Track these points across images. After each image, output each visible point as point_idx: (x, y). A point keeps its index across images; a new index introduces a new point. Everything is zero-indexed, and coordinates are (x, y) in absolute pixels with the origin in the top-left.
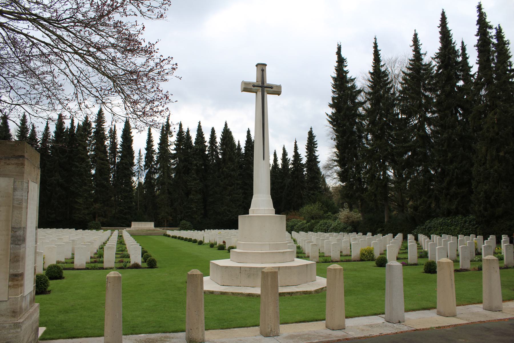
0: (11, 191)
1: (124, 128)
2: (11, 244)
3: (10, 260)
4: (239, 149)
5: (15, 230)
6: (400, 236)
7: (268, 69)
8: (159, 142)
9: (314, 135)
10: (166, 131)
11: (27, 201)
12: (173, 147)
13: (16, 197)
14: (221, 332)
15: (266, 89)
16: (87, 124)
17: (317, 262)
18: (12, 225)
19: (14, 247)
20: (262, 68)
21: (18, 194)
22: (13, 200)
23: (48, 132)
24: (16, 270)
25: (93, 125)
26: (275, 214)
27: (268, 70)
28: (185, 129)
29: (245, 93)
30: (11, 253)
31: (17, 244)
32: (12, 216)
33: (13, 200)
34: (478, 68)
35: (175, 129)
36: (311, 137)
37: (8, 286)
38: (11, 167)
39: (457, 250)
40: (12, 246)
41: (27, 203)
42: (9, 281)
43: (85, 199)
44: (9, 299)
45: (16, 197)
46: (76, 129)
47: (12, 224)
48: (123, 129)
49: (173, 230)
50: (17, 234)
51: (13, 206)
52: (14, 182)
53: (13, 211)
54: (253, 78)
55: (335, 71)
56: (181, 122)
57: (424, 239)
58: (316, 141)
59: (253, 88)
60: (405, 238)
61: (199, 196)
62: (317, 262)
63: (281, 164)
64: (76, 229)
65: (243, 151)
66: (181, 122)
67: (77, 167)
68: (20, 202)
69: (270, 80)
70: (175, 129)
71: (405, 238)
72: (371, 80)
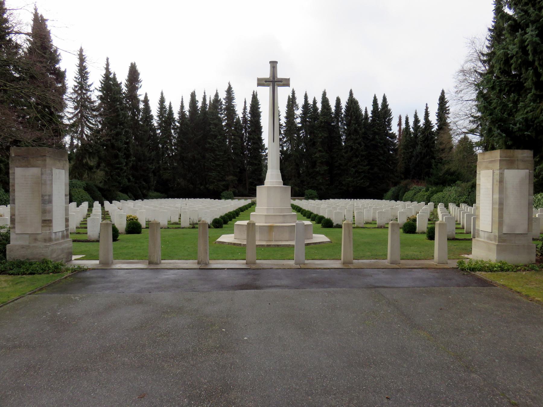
1: (251, 103)
2: (42, 204)
7: (278, 65)
8: (285, 115)
9: (446, 100)
10: (292, 102)
12: (298, 120)
15: (276, 83)
16: (217, 100)
20: (274, 64)
21: (44, 177)
23: (184, 111)
25: (224, 102)
26: (283, 185)
27: (279, 67)
28: (311, 102)
29: (259, 87)
35: (300, 102)
36: (442, 101)
38: (39, 162)
39: (353, 213)
40: (42, 205)
43: (367, 165)
44: (42, 233)
46: (208, 107)
48: (251, 105)
49: (301, 200)
51: (42, 183)
52: (42, 170)
54: (267, 75)
57: (465, 207)
58: (449, 107)
59: (265, 83)
61: (326, 168)
64: (215, 199)
67: (210, 143)
69: (280, 75)
70: (300, 102)
72: (489, 38)
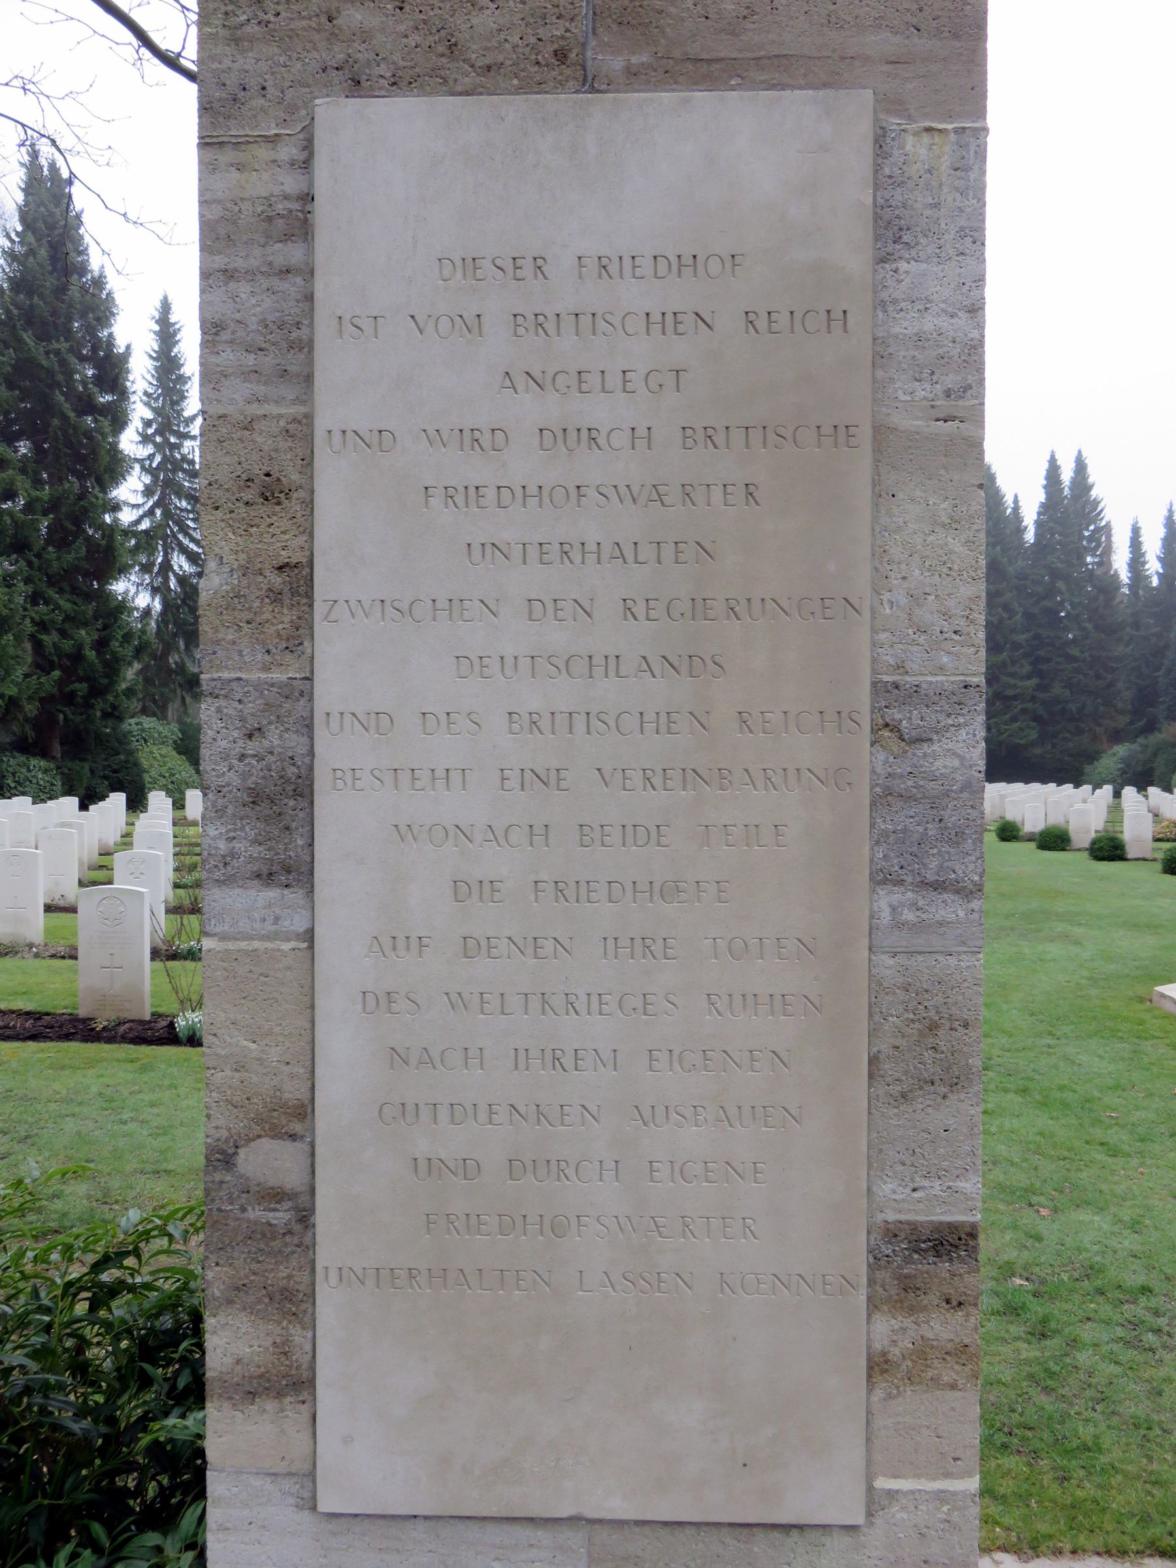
2: (882, 878)
3: (873, 1061)
4: (1020, 530)
5: (909, 719)
6: (1108, 789)
13: (905, 325)
14: (160, 1006)
18: (874, 671)
19: (909, 916)
22: (880, 355)
30: (877, 988)
31: (938, 886)
32: (880, 553)
37: (863, 1363)
40: (885, 900)
42: (873, 1305)
44: (874, 1502)
45: (905, 325)
51: (881, 432)
52: (881, 141)
53: (881, 494)
60: (1117, 794)
63: (1157, 573)
65: (1030, 536)
71: (1117, 794)
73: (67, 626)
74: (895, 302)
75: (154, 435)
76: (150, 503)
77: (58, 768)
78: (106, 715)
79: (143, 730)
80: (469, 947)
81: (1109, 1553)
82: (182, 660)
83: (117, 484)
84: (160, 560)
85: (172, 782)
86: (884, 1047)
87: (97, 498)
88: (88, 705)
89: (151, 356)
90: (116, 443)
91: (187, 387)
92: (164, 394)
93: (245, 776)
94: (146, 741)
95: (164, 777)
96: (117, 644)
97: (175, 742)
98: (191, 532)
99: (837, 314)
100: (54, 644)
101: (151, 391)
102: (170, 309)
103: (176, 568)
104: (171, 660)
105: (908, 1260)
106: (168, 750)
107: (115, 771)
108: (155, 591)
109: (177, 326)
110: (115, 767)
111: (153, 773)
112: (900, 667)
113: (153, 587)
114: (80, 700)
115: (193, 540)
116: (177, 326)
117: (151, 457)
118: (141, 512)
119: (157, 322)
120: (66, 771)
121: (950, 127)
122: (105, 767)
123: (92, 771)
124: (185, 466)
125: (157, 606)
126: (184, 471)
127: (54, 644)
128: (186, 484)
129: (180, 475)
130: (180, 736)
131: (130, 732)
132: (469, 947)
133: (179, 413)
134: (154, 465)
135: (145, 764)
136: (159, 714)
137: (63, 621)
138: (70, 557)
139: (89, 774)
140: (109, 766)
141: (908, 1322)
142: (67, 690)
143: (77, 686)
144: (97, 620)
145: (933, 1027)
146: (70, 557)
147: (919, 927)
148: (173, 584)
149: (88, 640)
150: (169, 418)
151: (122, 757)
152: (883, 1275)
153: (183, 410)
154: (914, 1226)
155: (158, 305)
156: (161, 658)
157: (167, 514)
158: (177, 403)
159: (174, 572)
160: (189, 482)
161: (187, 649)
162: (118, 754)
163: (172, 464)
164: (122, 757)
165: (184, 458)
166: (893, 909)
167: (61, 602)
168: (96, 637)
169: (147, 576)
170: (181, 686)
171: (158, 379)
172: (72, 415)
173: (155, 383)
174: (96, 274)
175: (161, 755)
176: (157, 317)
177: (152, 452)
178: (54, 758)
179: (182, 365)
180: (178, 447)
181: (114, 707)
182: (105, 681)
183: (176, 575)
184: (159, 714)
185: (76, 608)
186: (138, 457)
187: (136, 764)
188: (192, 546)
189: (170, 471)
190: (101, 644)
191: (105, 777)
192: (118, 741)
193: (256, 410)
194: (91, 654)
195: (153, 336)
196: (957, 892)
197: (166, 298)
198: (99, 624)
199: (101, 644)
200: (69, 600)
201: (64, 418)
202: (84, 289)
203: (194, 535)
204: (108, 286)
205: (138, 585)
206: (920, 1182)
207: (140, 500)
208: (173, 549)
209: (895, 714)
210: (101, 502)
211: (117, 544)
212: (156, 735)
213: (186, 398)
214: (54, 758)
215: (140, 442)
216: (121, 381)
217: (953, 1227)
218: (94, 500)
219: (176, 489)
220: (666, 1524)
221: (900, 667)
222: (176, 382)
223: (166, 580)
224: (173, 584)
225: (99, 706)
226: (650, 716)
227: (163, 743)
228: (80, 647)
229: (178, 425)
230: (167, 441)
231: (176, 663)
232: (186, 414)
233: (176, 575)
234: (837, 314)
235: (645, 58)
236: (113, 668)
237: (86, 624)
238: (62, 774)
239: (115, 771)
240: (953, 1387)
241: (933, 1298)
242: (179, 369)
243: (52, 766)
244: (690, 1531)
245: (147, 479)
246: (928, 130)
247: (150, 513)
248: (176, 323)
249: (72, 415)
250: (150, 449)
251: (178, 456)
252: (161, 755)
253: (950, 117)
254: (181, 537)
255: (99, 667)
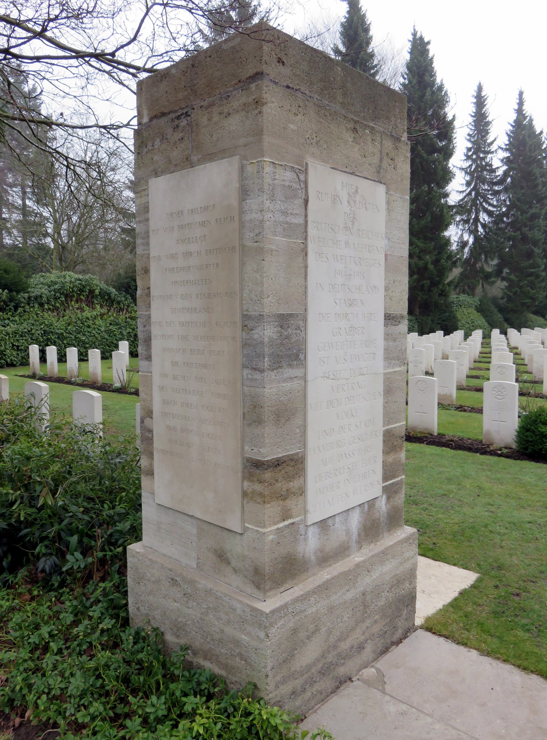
0: (235, 202)
2: (244, 366)
3: (244, 414)
5: (250, 324)
11: (306, 232)
17: (488, 379)
19: (250, 377)
22: (242, 225)
24: (256, 450)
31: (255, 369)
33: (242, 225)
34: (448, 87)
40: (246, 372)
41: (306, 239)
47: (241, 304)
50: (256, 336)
52: (242, 169)
55: (409, 46)
56: (442, 80)
60: (487, 336)
62: (488, 379)
66: (442, 80)
68: (257, 231)
71: (487, 336)
73: (421, 254)
74: (246, 211)
75: (472, 155)
76: (469, 189)
77: (417, 319)
78: (440, 295)
79: (460, 301)
80: (175, 378)
81: (519, 667)
82: (482, 265)
83: (447, 183)
84: (473, 217)
85: (473, 326)
86: (246, 411)
87: (436, 192)
88: (430, 290)
89: (472, 116)
90: (447, 164)
91: (489, 127)
92: (478, 133)
93: (144, 336)
94: (461, 306)
95: (469, 323)
96: (444, 261)
97: (476, 306)
98: (489, 201)
99: (232, 217)
100: (415, 263)
101: (471, 133)
102: (482, 89)
103: (481, 220)
104: (477, 266)
105: (251, 468)
106: (472, 310)
107: (444, 321)
108: (471, 232)
109: (485, 97)
110: (444, 319)
111: (463, 322)
112: (247, 310)
113: (470, 230)
114: (426, 288)
115: (490, 205)
116: (485, 97)
117: (470, 166)
118: (464, 194)
119: (475, 97)
120: (420, 321)
121: (255, 161)
122: (439, 319)
123: (432, 321)
124: (488, 168)
125: (471, 241)
126: (487, 170)
127: (415, 263)
128: (488, 177)
129: (485, 173)
130: (479, 303)
131: (453, 302)
132: (175, 378)
133: (485, 141)
134: (472, 170)
135: (459, 317)
136: (470, 293)
137: (420, 252)
138: (423, 222)
139: (431, 322)
140: (441, 319)
141: (251, 484)
142: (421, 284)
143: (425, 282)
144: (435, 250)
145: (255, 407)
146: (423, 222)
147: (252, 380)
148: (480, 229)
149: (430, 261)
150: (479, 145)
151: (447, 314)
152: (246, 471)
153: (487, 139)
154: (252, 459)
155: (476, 88)
156: (472, 265)
157: (478, 194)
158: (484, 136)
159: (480, 222)
160: (489, 175)
161: (486, 260)
162: (445, 312)
163: (480, 167)
164: (447, 314)
165: (487, 164)
166: (247, 375)
167: (419, 244)
168: (434, 258)
169: (467, 226)
170: (482, 278)
171: (475, 126)
172: (425, 155)
173: (473, 128)
174: (440, 84)
175: (468, 313)
176: (475, 95)
177: (471, 163)
178: (415, 315)
179: (488, 116)
180: (483, 159)
181: (443, 291)
182: (438, 279)
183: (481, 224)
184: (470, 293)
185: (426, 245)
186: (464, 167)
187: (455, 317)
188: (490, 208)
189: (480, 171)
190: (436, 262)
191: (438, 323)
192: (447, 307)
193: (144, 252)
194: (431, 267)
195: (473, 105)
196: (259, 371)
197: (480, 84)
198: (436, 252)
199: (436, 262)
200: (422, 242)
201: (422, 157)
202: (433, 93)
203: (491, 202)
204: (445, 89)
205: (463, 230)
206: (254, 448)
207: (464, 188)
208: (480, 211)
209: (247, 323)
210: (438, 194)
211: (445, 213)
212: (466, 303)
213: (489, 133)
214: (415, 315)
215: (465, 160)
216: (449, 134)
217: (259, 461)
218: (435, 194)
219: (482, 180)
220: (209, 523)
221: (247, 310)
222: (484, 126)
223: (477, 226)
224: (480, 229)
225: (435, 290)
226: (201, 323)
227: (470, 307)
228: (426, 264)
229: (485, 148)
230: (478, 157)
231: (480, 267)
232: (488, 141)
233: (481, 224)
234: (232, 217)
235: (200, 156)
236: (442, 272)
237: (430, 253)
238: (418, 322)
239: (444, 321)
240: (259, 503)
241: (255, 479)
242: (486, 119)
243: (414, 318)
244: (213, 526)
245: (468, 178)
246: (251, 163)
247: (470, 194)
248: (485, 96)
249: (425, 155)
250: (470, 163)
251: (484, 163)
252: (468, 313)
253: (256, 158)
254: (484, 204)
255: (435, 272)
